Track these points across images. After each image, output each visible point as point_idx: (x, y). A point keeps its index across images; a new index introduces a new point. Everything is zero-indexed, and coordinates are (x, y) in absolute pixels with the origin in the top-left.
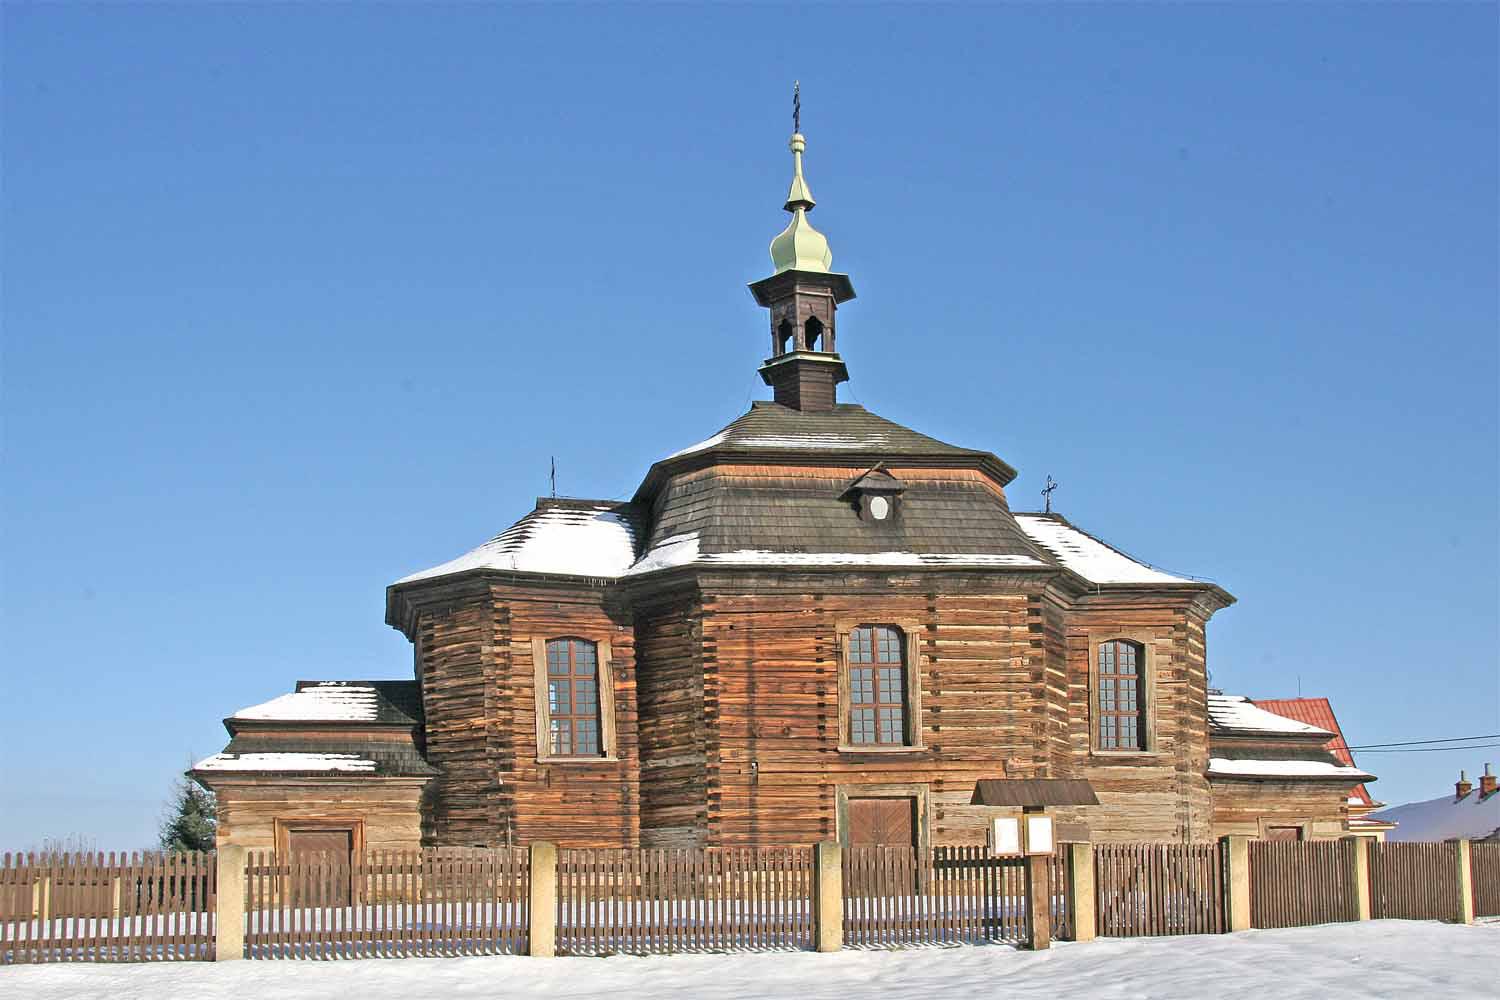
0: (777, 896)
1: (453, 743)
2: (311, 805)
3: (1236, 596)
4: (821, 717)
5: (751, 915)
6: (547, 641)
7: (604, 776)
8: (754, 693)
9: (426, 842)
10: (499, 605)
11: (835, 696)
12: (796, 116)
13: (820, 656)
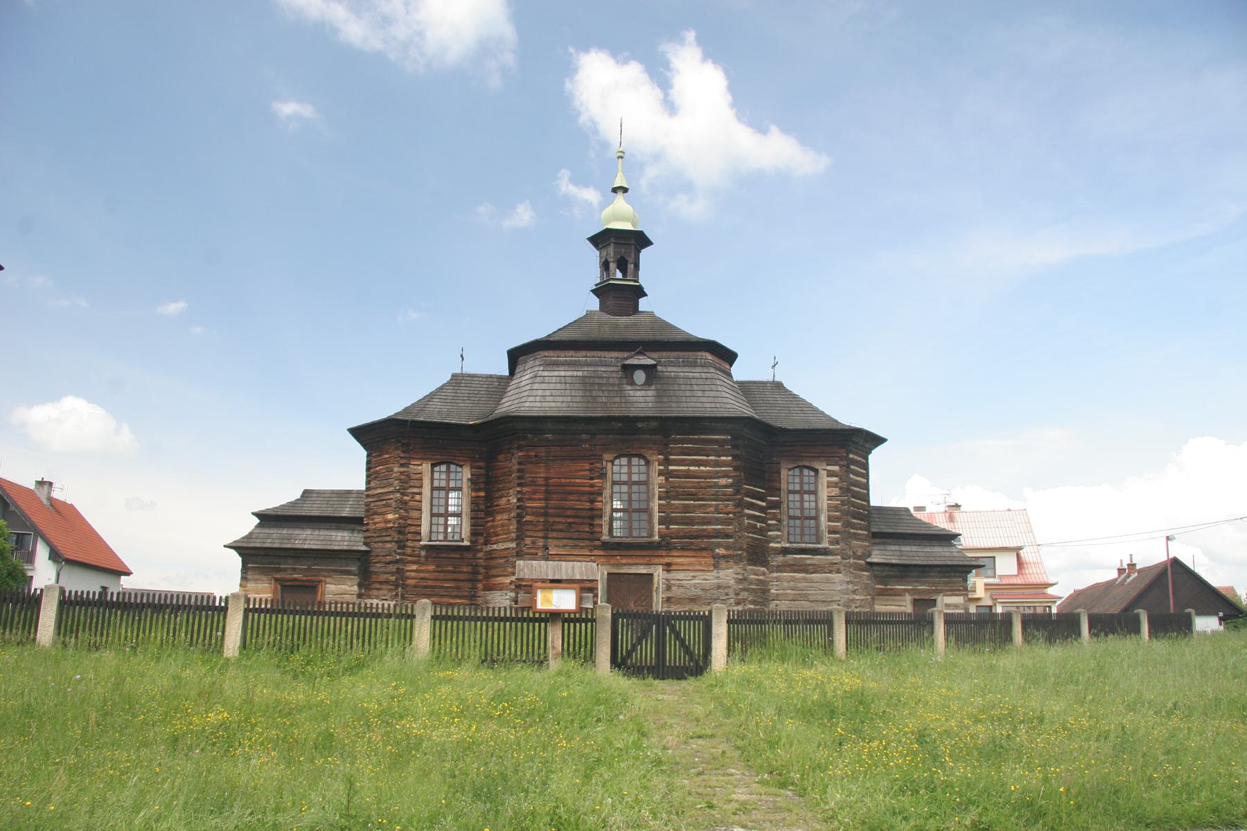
1: (375, 531)
2: (294, 569)
3: (131, 569)
9: (360, 596)
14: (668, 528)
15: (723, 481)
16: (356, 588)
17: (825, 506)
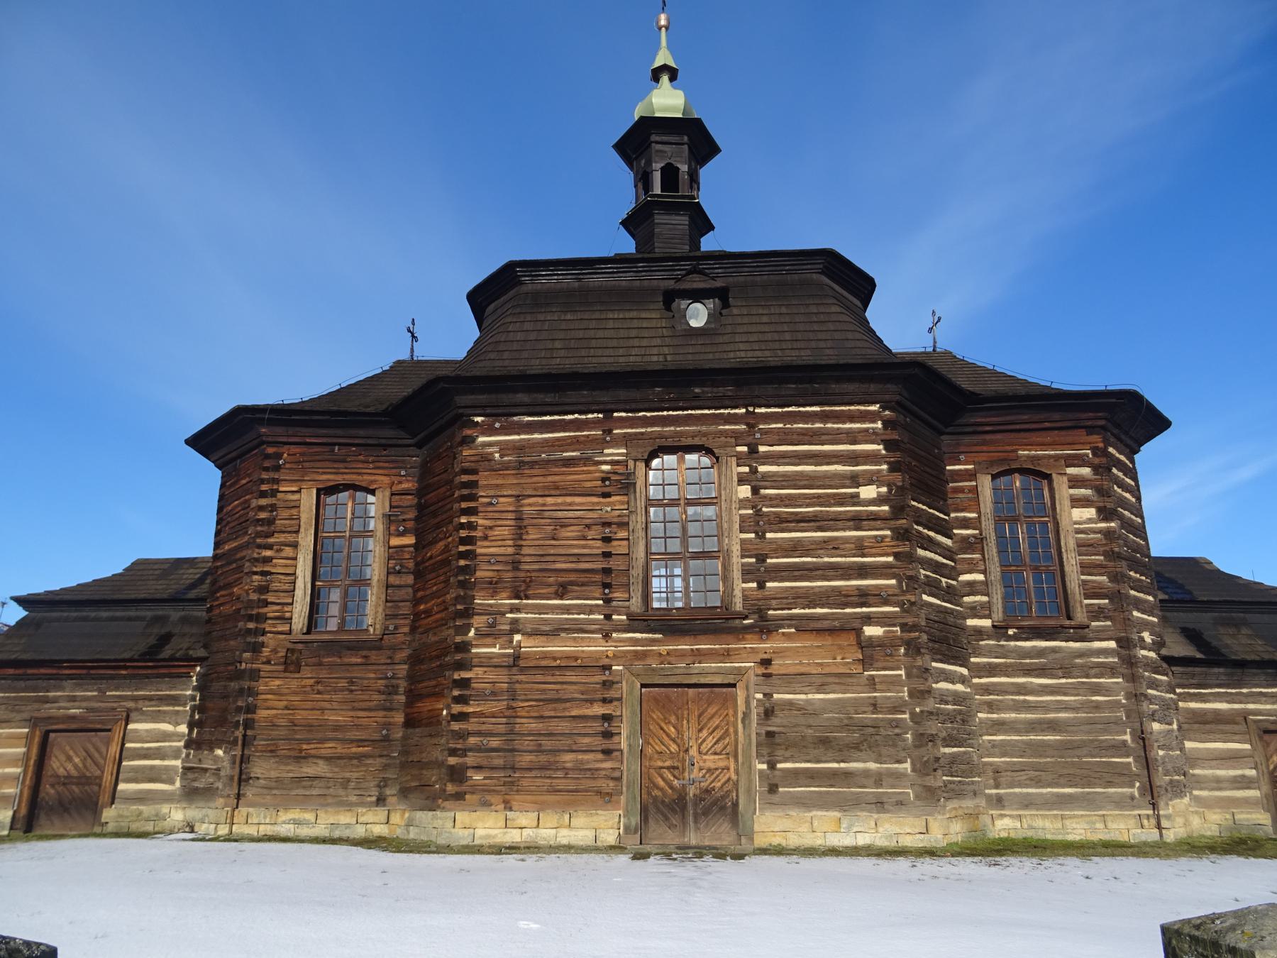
2: (73, 699)
7: (366, 657)
8: (521, 539)
10: (270, 450)
11: (625, 543)
13: (607, 490)
14: (761, 586)
15: (868, 492)
16: (183, 729)
17: (1072, 544)
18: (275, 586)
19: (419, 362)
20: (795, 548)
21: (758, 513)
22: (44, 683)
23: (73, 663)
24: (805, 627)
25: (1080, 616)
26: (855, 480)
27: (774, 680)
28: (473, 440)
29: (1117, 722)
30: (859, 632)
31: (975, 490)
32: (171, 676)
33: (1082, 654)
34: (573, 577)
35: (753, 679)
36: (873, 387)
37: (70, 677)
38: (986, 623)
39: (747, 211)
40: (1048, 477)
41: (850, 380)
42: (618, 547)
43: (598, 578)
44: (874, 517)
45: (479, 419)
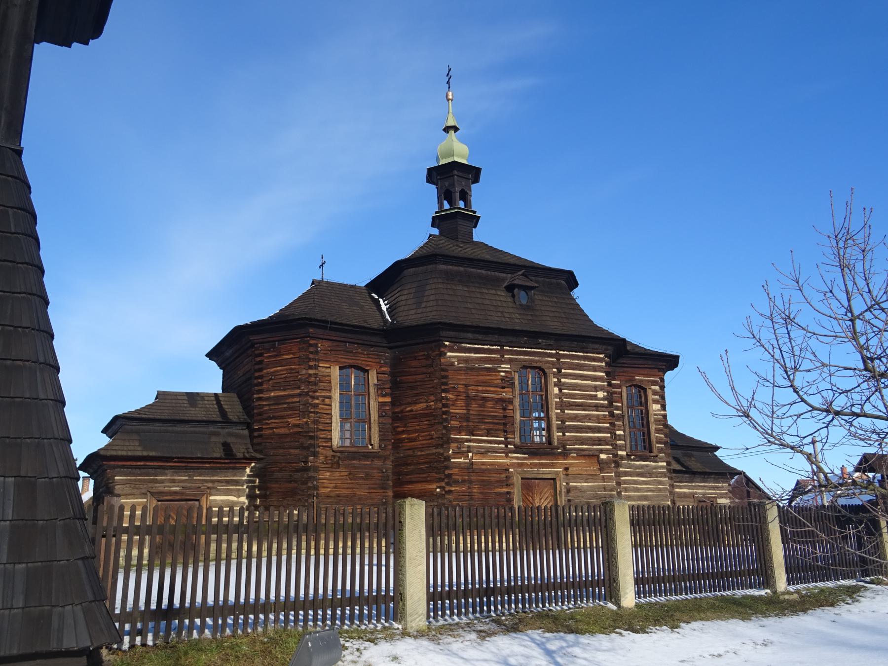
0: (591, 548)
2: (173, 481)
4: (505, 424)
5: (648, 572)
6: (340, 368)
12: (448, 82)
14: (564, 435)
15: (600, 394)
18: (322, 420)
19: (327, 283)
20: (575, 418)
21: (562, 401)
22: (152, 471)
23: (181, 459)
24: (581, 454)
25: (655, 452)
26: (596, 388)
27: (570, 477)
28: (445, 354)
29: (666, 496)
30: (598, 457)
31: (621, 393)
32: (234, 468)
33: (656, 468)
34: (491, 426)
35: (562, 476)
36: (604, 347)
37: (171, 468)
38: (624, 453)
39: (502, 227)
40: (645, 390)
41: (597, 343)
42: (509, 413)
43: (502, 427)
44: (603, 406)
45: (447, 343)
